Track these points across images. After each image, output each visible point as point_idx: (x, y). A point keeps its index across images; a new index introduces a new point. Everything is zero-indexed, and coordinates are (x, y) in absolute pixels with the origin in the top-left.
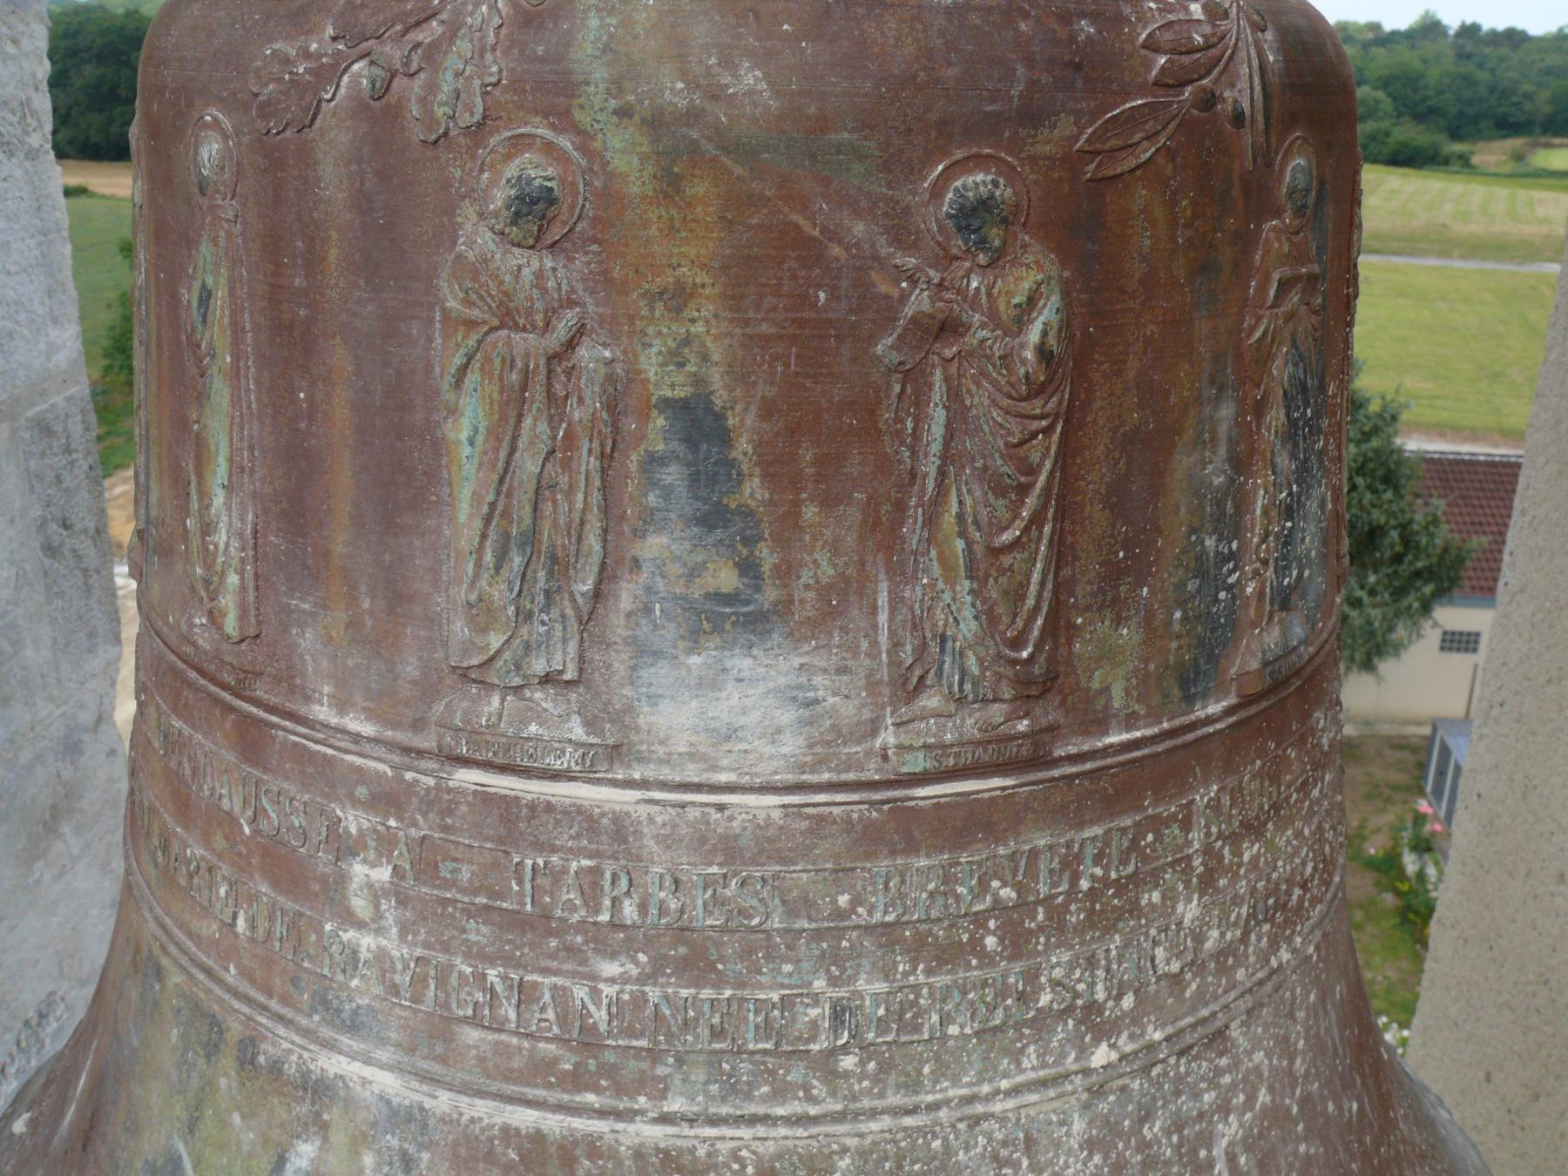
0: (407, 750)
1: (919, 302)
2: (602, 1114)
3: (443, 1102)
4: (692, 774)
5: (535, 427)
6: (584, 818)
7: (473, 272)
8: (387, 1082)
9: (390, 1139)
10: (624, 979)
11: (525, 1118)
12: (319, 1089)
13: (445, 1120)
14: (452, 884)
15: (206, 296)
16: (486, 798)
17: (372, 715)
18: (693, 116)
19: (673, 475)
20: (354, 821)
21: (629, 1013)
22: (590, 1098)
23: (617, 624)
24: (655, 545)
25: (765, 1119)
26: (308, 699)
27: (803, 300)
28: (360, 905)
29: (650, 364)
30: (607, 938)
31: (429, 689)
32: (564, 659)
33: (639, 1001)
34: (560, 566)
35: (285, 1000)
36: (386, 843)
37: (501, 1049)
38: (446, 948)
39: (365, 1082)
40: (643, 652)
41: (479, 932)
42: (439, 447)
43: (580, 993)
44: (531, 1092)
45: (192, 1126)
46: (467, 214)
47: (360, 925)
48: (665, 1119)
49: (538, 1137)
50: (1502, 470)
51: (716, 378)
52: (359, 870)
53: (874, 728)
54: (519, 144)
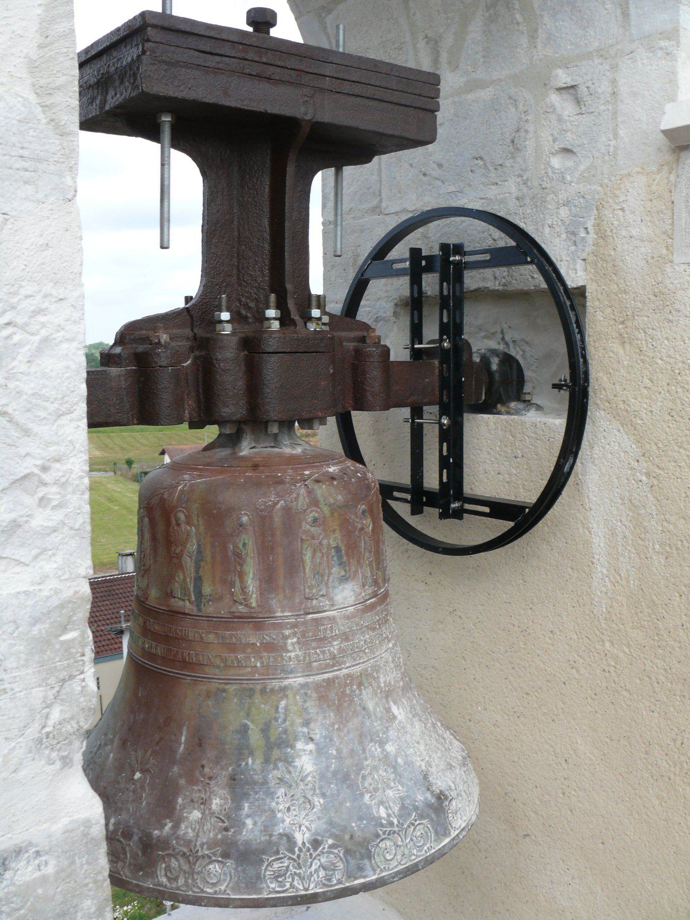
0: (297, 615)
1: (359, 526)
2: (337, 670)
3: (310, 679)
4: (342, 606)
5: (319, 554)
6: (329, 618)
7: (307, 532)
8: (301, 680)
9: (302, 691)
10: (338, 644)
11: (326, 676)
12: (284, 689)
13: (312, 682)
14: (308, 637)
15: (244, 545)
16: (313, 619)
17: (289, 611)
18: (334, 503)
19: (335, 558)
20: (287, 632)
21: (341, 650)
22: (336, 668)
23: (330, 584)
24: (334, 570)
25: (359, 664)
26: (274, 613)
27: (348, 529)
28: (290, 648)
29: (331, 542)
30: (334, 638)
31: (301, 603)
32: (323, 592)
33: (341, 647)
34: (322, 576)
35: (274, 674)
36: (295, 634)
37: (320, 665)
38: (308, 649)
39: (295, 682)
40: (334, 587)
41: (314, 644)
42: (303, 561)
43: (332, 649)
44: (328, 670)
45: (248, 715)
46: (304, 524)
47: (291, 652)
48: (347, 668)
49: (329, 679)
50: (127, 581)
51: (339, 542)
52: (290, 641)
53: (361, 593)
54: (312, 511)
